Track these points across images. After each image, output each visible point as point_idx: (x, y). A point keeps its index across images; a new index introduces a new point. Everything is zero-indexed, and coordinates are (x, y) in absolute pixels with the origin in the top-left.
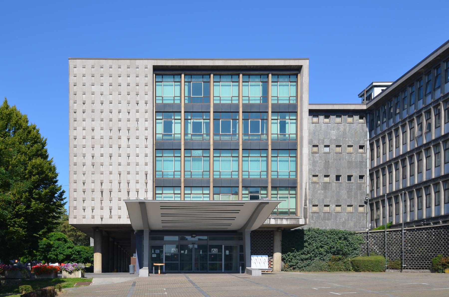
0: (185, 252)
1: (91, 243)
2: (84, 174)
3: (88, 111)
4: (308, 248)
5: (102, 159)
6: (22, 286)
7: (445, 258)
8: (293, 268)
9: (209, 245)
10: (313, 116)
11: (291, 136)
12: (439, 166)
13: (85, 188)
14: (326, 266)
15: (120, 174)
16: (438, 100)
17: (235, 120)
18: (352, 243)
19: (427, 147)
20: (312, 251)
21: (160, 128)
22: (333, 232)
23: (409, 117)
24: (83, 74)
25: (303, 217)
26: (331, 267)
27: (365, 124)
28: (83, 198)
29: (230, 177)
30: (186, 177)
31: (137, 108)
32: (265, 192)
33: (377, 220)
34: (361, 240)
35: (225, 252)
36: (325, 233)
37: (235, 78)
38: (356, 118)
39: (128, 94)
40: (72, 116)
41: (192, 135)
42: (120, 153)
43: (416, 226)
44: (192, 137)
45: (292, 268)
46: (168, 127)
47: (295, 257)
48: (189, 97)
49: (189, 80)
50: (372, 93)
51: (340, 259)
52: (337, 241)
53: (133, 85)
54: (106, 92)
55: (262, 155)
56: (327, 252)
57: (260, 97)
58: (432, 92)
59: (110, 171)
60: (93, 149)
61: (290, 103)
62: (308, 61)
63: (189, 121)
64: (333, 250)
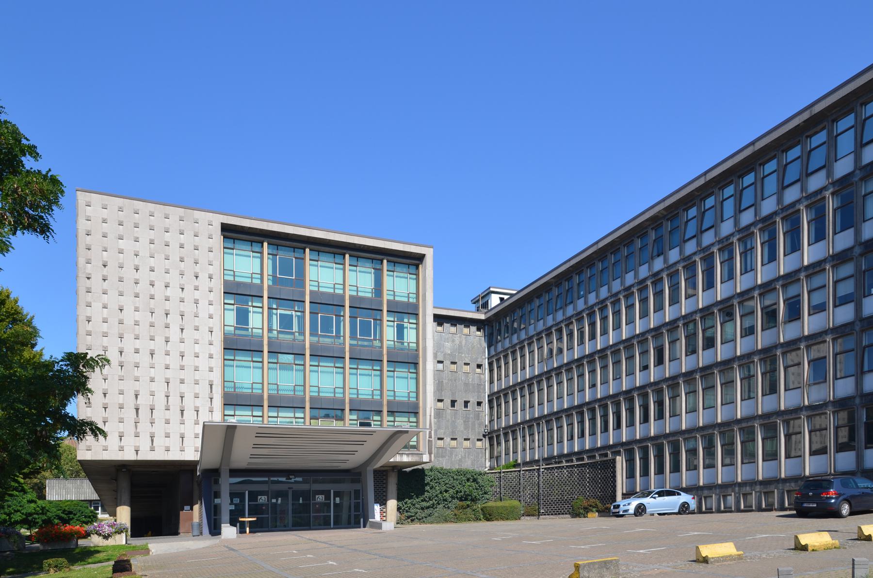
0: (277, 500)
1: (47, 495)
2: (105, 379)
3: (113, 279)
4: (429, 492)
5: (137, 358)
6: (48, 560)
7: (587, 500)
8: (412, 519)
9: (312, 491)
10: (438, 324)
11: (411, 345)
12: (572, 394)
13: (106, 402)
14: (452, 516)
15: (168, 383)
16: (570, 318)
17: (338, 316)
18: (483, 486)
19: (558, 372)
20: (434, 497)
21: (231, 318)
22: (459, 472)
23: (536, 334)
24: (103, 218)
25: (427, 453)
26: (458, 516)
27: (483, 338)
28: (103, 417)
29: (332, 395)
30: (226, 390)
31: (196, 283)
32: (378, 418)
33: (498, 458)
34: (492, 482)
35: (334, 499)
36: (450, 473)
37: (339, 259)
38: (473, 329)
39: (182, 260)
40: (83, 283)
41: (279, 332)
42: (168, 349)
43: (546, 465)
44: (236, 331)
45: (409, 520)
46: (242, 317)
47: (414, 505)
48: (274, 276)
49: (275, 252)
50: (489, 301)
51: (468, 506)
52: (465, 483)
53: (189, 247)
54: (144, 253)
55: (375, 368)
56: (453, 497)
57: (372, 289)
58: (564, 307)
59: (150, 377)
60: (121, 341)
61: (410, 301)
62: (432, 249)
63: (274, 311)
64: (459, 495)
